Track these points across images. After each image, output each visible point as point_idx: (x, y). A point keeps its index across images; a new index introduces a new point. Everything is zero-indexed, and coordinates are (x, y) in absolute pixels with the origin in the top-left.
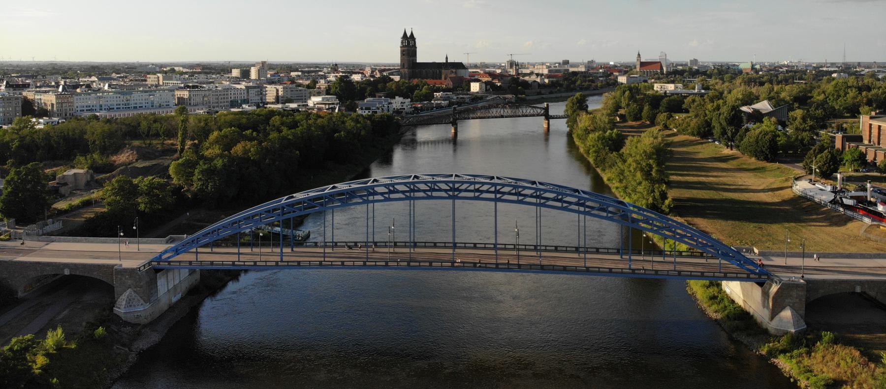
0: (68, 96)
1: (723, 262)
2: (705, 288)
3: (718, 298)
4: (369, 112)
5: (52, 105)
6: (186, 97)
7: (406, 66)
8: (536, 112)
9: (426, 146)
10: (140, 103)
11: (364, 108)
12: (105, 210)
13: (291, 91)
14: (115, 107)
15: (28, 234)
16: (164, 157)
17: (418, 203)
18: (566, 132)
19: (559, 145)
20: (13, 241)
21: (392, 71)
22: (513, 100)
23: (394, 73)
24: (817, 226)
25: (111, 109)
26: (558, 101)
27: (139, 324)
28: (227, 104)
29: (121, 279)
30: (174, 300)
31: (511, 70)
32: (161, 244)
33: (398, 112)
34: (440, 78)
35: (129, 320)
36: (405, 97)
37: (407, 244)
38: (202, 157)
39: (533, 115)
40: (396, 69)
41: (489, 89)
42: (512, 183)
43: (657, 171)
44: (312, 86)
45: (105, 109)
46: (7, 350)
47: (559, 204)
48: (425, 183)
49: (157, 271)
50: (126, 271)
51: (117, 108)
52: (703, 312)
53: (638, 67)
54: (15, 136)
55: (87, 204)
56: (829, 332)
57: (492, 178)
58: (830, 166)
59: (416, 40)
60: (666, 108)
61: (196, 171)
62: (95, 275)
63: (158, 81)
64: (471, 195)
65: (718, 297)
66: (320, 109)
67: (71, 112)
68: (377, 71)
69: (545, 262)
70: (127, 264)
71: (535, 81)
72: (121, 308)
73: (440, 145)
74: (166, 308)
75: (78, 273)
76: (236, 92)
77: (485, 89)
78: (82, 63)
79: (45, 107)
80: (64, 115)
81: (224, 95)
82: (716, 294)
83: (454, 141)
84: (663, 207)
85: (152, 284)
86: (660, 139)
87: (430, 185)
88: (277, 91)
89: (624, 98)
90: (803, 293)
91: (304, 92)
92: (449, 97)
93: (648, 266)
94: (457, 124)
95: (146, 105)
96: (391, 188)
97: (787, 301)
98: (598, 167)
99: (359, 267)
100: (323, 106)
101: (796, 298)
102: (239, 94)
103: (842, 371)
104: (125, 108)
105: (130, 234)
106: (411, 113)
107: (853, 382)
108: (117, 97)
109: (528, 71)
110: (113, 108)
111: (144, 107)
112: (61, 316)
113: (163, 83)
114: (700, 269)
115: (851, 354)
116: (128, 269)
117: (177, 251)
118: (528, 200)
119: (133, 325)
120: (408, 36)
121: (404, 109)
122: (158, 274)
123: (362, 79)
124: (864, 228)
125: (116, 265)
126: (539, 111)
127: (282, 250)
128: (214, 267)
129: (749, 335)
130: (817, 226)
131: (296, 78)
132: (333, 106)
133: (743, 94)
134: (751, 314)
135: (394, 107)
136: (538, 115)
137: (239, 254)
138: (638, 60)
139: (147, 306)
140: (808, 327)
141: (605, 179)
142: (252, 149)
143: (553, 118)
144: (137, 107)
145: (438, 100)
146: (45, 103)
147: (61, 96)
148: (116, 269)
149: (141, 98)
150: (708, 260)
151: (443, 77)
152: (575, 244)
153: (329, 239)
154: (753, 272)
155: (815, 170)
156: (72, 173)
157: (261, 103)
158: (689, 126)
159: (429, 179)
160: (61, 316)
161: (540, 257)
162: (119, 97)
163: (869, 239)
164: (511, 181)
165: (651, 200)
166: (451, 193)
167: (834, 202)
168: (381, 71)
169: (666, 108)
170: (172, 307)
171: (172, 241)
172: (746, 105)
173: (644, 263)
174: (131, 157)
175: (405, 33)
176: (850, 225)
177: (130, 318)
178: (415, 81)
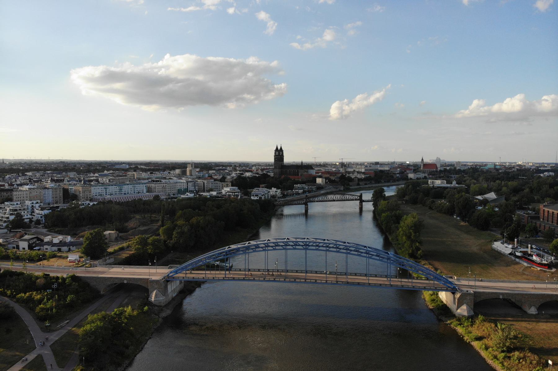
0: (88, 187)
1: (436, 282)
2: (430, 296)
3: (436, 299)
4: (257, 198)
8: (354, 198)
10: (128, 191)
11: (254, 195)
12: (133, 252)
13: (212, 184)
14: (114, 193)
15: (100, 264)
17: (289, 251)
18: (372, 211)
19: (368, 216)
21: (269, 170)
23: (270, 171)
25: (112, 194)
27: (161, 306)
28: (176, 191)
29: (152, 285)
30: (174, 295)
31: (342, 169)
32: (166, 269)
33: (273, 197)
35: (156, 304)
36: (278, 188)
37: (283, 271)
38: (176, 225)
40: (271, 169)
41: (328, 182)
42: (334, 243)
44: (223, 180)
45: (108, 194)
46: (113, 314)
47: (356, 253)
48: (293, 242)
49: (168, 281)
50: (154, 281)
51: (115, 194)
53: (422, 167)
55: (122, 249)
56: (482, 316)
57: (325, 240)
59: (284, 152)
61: (174, 233)
62: (139, 283)
63: (134, 176)
64: (314, 248)
66: (229, 195)
67: (90, 196)
69: (349, 281)
70: (154, 278)
72: (153, 298)
73: (298, 217)
74: (171, 299)
76: (181, 184)
77: (325, 182)
78: (79, 161)
80: (86, 198)
82: (435, 299)
83: (306, 214)
84: (417, 255)
86: (416, 219)
87: (294, 243)
90: (472, 298)
91: (219, 184)
92: (303, 187)
93: (410, 284)
96: (276, 244)
97: (464, 301)
98: (387, 232)
99: (261, 281)
100: (231, 193)
101: (469, 300)
102: (182, 185)
103: (485, 333)
104: (120, 194)
105: (153, 264)
106: (281, 198)
107: (488, 338)
108: (115, 188)
109: (352, 170)
110: (113, 194)
111: (130, 193)
112: (125, 302)
113: (137, 178)
114: (425, 285)
115: (491, 326)
116: (155, 280)
117: (176, 272)
118: (342, 251)
119: (158, 306)
120: (279, 149)
121: (277, 195)
122: (168, 283)
124: (522, 269)
125: (149, 278)
126: (356, 197)
127: (225, 273)
128: (195, 280)
129: (446, 317)
131: (213, 175)
132: (237, 193)
134: (450, 308)
135: (271, 194)
137: (206, 274)
138: (422, 163)
139: (164, 297)
140: (474, 314)
141: (390, 239)
142: (201, 221)
143: (365, 202)
144: (126, 193)
145: (296, 189)
148: (150, 280)
150: (430, 281)
152: (386, 274)
153: (247, 268)
154: (449, 287)
155: (506, 236)
157: (195, 190)
158: (443, 208)
159: (294, 240)
160: (125, 302)
161: (347, 278)
162: (116, 188)
163: (524, 274)
164: (334, 241)
165: (410, 251)
166: (305, 247)
167: (510, 254)
168: (262, 170)
170: (173, 299)
171: (171, 268)
172: (480, 195)
173: (406, 283)
175: (277, 148)
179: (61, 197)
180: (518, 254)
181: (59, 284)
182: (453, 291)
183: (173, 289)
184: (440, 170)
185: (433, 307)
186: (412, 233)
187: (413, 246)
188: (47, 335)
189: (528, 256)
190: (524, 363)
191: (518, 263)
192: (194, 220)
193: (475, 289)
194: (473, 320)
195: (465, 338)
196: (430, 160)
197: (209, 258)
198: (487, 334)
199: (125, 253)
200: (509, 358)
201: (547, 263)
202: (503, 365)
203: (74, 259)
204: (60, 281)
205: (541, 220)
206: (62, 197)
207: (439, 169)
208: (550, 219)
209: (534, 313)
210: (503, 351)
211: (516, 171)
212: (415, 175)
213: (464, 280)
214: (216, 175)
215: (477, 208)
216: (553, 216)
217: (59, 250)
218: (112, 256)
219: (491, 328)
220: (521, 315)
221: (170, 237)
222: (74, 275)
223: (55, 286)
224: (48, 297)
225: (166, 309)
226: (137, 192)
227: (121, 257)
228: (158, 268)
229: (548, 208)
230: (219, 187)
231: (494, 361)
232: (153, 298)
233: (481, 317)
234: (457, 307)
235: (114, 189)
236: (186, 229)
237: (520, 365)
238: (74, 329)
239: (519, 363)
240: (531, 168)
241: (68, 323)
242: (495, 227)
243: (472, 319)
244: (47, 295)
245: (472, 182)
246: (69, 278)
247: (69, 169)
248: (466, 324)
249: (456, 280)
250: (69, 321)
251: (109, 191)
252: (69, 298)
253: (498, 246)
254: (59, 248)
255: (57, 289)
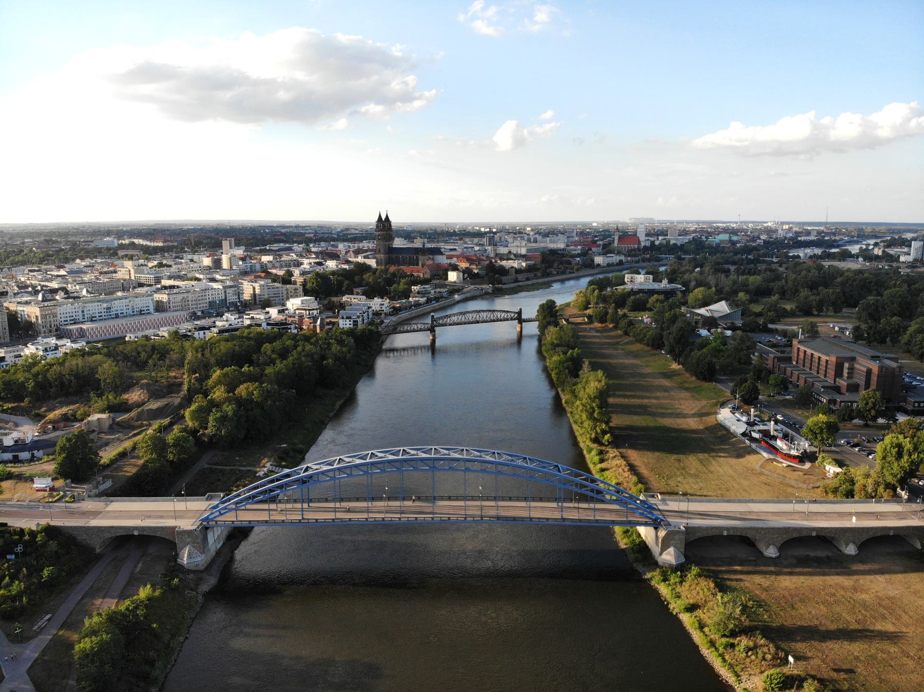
5: (37, 317)
6: (165, 300)
7: (382, 251)
9: (406, 352)
10: (121, 310)
11: (345, 317)
15: (89, 496)
16: (173, 395)
20: (78, 503)
22: (490, 291)
23: (370, 256)
26: (534, 290)
28: (206, 305)
30: (219, 546)
34: (417, 265)
35: (190, 569)
39: (507, 320)
43: (599, 413)
49: (207, 528)
52: (616, 543)
54: (27, 375)
58: (751, 395)
60: (631, 306)
62: (158, 534)
63: (130, 274)
65: (629, 531)
67: (56, 323)
68: (351, 252)
71: (512, 267)
75: (145, 533)
79: (28, 319)
81: (202, 296)
84: (603, 441)
85: (205, 539)
86: (603, 383)
88: (254, 288)
89: (593, 296)
90: (683, 537)
94: (435, 331)
95: (127, 311)
100: (304, 311)
107: (705, 606)
108: (98, 306)
112: (138, 569)
119: (195, 572)
120: (383, 219)
123: (337, 266)
127: (302, 505)
129: (644, 565)
131: (269, 265)
133: (703, 295)
136: (512, 319)
139: (203, 556)
141: (563, 401)
142: (255, 392)
143: (526, 322)
146: (28, 316)
147: (45, 308)
149: (121, 305)
151: (420, 264)
156: (96, 418)
160: (138, 569)
165: (593, 436)
167: (744, 434)
169: (631, 306)
170: (218, 553)
174: (142, 395)
175: (380, 217)
176: (751, 458)
177: (192, 567)
178: (393, 269)
179: (5, 329)
180: (756, 435)
181: (26, 544)
182: (656, 526)
183: (215, 540)
184: (645, 247)
185: (626, 544)
186: (596, 409)
187: (597, 429)
188: (16, 649)
189: (770, 439)
190: (753, 657)
191: (755, 452)
192: (242, 390)
193: (688, 518)
194: (683, 574)
195: (671, 607)
196: (630, 219)
197: (271, 476)
198: (703, 601)
199: (130, 464)
200: (732, 646)
201: (797, 454)
202: (724, 660)
203: (45, 486)
204: (27, 537)
205: (794, 363)
206: (7, 328)
207: (643, 244)
208: (808, 365)
209: (774, 556)
210: (724, 636)
211: (762, 244)
212: (605, 258)
213: (671, 501)
214: (274, 267)
215: (698, 331)
216: (811, 360)
217: (16, 460)
218: (107, 473)
219: (709, 589)
220: (754, 559)
221: (204, 425)
222: (49, 526)
223: (19, 549)
224: (12, 571)
225: (209, 575)
226: (138, 310)
227: (124, 473)
228: (188, 501)
229: (805, 346)
230: (281, 295)
231: (711, 652)
232: (185, 559)
233: (695, 570)
234: (661, 548)
235: (97, 308)
236: (229, 409)
237: (748, 660)
238: (61, 633)
239: (748, 657)
240: (786, 238)
241: (49, 620)
242: (725, 375)
243: (681, 569)
244: (8, 569)
245: (693, 278)
246: (42, 533)
247: (14, 252)
248: (672, 581)
249: (661, 501)
250: (50, 615)
251: (88, 312)
252: (46, 573)
253: (725, 415)
254: (14, 454)
255: (24, 554)
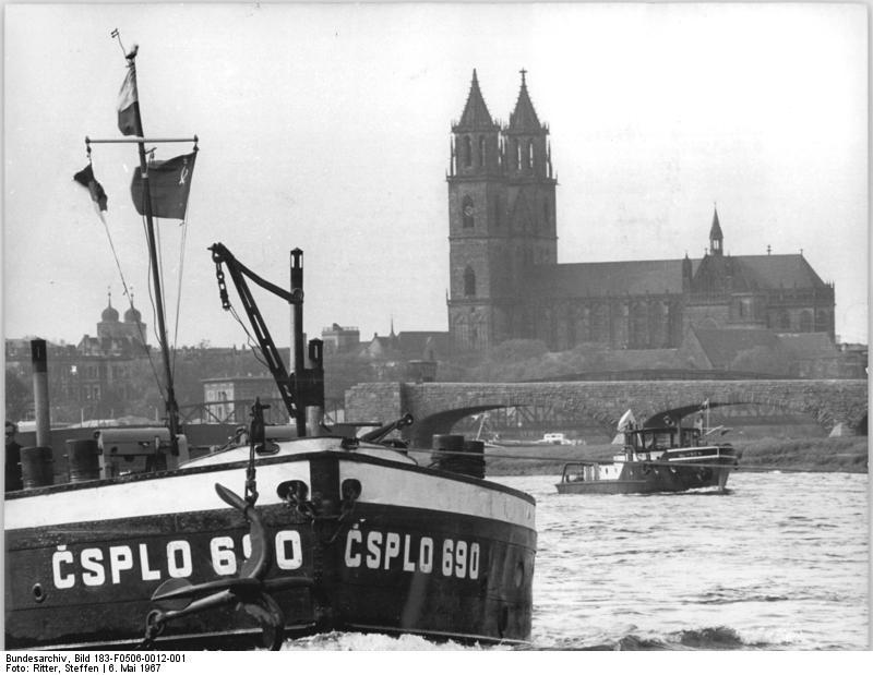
24: (714, 610)
130: (714, 610)
175: (476, 102)
